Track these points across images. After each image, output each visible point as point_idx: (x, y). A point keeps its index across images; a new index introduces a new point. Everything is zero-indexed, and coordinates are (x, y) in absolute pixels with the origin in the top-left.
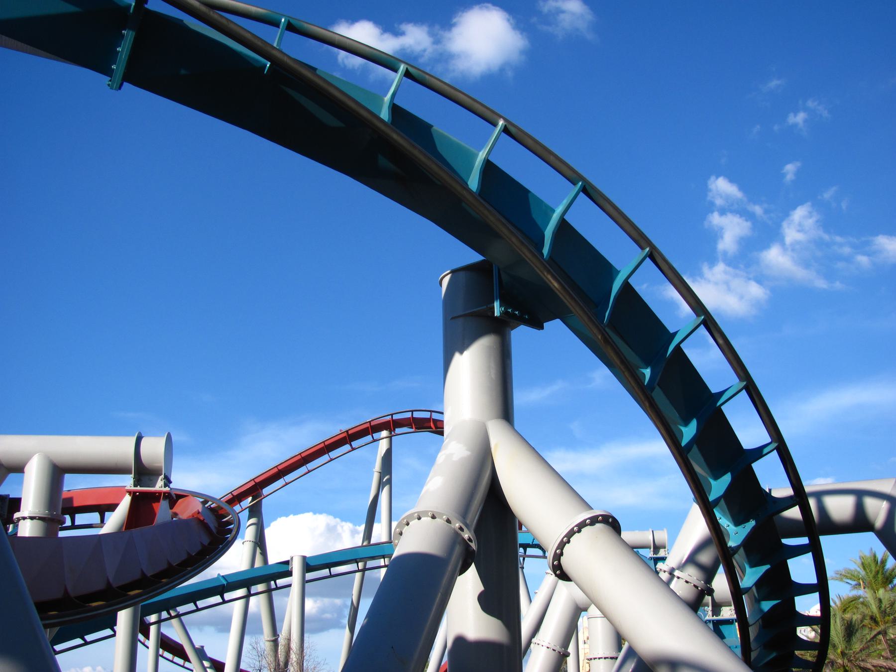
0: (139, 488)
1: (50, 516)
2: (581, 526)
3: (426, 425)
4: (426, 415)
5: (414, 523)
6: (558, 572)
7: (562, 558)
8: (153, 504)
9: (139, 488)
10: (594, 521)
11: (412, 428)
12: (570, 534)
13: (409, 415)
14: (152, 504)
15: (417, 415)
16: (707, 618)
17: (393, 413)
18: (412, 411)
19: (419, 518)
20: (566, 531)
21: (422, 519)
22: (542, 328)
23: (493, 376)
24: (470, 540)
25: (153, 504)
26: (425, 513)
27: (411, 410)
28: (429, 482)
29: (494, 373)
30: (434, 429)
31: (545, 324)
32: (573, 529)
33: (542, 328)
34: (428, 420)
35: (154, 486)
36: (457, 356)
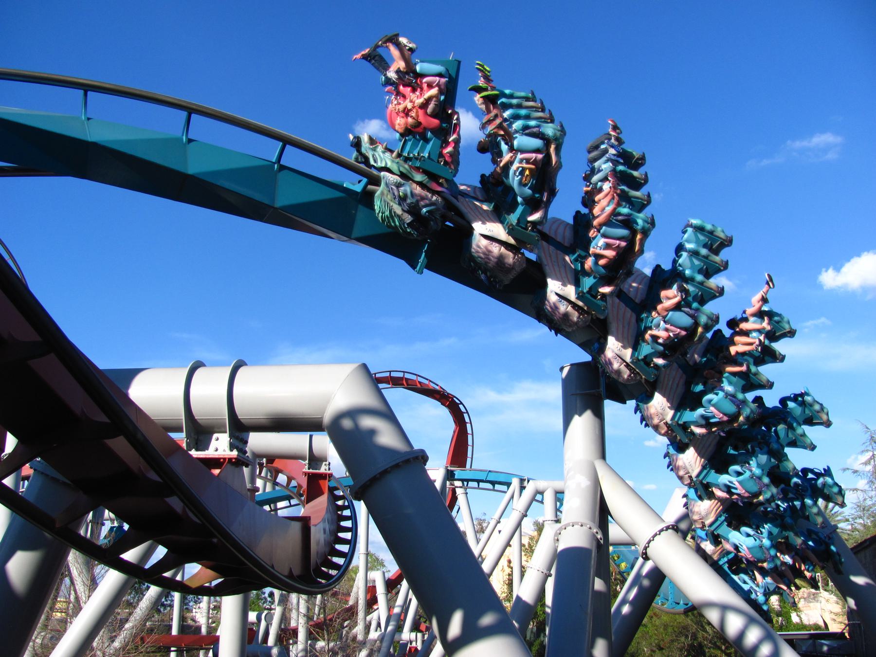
0: (311, 471)
1: (252, 488)
2: (661, 531)
3: (401, 382)
4: (401, 375)
5: (569, 528)
6: (644, 556)
7: (648, 548)
8: (320, 481)
9: (311, 471)
10: (668, 528)
11: (389, 384)
12: (655, 535)
13: (387, 374)
14: (318, 482)
15: (394, 374)
16: (304, 470)
17: (376, 372)
18: (390, 372)
19: (573, 526)
20: (653, 534)
21: (575, 526)
22: (626, 403)
23: (597, 432)
24: (601, 539)
25: (320, 481)
26: (577, 523)
27: (389, 370)
28: (26, 282)
29: (598, 431)
30: (406, 386)
31: (627, 402)
32: (656, 533)
33: (626, 403)
34: (401, 379)
35: (319, 470)
36: (576, 418)
